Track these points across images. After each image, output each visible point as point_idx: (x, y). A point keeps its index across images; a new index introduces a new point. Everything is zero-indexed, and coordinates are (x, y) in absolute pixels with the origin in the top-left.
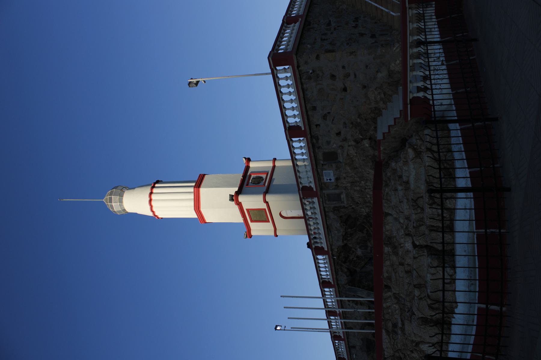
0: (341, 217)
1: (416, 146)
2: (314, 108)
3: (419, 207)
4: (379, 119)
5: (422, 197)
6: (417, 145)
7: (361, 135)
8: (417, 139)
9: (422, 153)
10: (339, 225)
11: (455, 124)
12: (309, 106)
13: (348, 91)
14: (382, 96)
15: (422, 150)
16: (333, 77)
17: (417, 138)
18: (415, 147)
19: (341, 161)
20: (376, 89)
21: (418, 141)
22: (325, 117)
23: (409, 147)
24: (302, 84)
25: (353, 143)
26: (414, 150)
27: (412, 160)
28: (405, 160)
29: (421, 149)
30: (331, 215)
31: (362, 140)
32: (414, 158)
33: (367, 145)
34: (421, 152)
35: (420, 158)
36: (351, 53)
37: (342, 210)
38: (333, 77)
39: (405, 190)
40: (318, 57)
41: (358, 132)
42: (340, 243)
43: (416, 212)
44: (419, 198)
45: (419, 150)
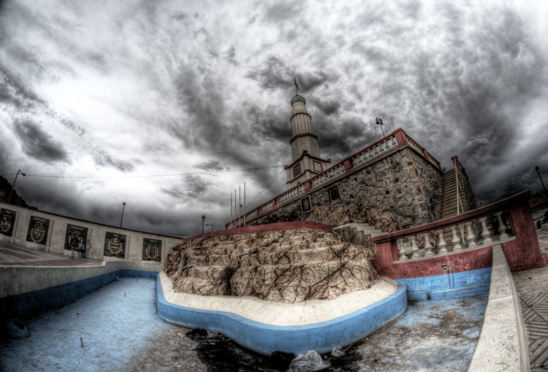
0: (295, 212)
1: (348, 251)
2: (369, 173)
3: (279, 259)
4: (367, 224)
5: (290, 262)
6: (348, 253)
7: (353, 214)
8: (355, 251)
9: (339, 259)
10: (290, 211)
11: (190, 307)
12: (370, 168)
13: (386, 196)
14: (387, 224)
15: (343, 258)
16: (397, 180)
17: (357, 252)
18: (346, 251)
19: (332, 203)
20: (391, 218)
21: (353, 253)
22: (363, 182)
23: (345, 245)
24: (386, 158)
25: (346, 209)
26: (343, 250)
27: (331, 249)
28: (331, 243)
29: (344, 257)
30: (295, 205)
31: (349, 216)
32: (334, 251)
33: (345, 220)
34: (340, 257)
35: (333, 258)
36: (419, 190)
37: (299, 212)
38: (397, 180)
39: (301, 246)
40: (410, 164)
41: (355, 211)
42: (279, 215)
43: (273, 256)
44: (289, 259)
45: (343, 255)
